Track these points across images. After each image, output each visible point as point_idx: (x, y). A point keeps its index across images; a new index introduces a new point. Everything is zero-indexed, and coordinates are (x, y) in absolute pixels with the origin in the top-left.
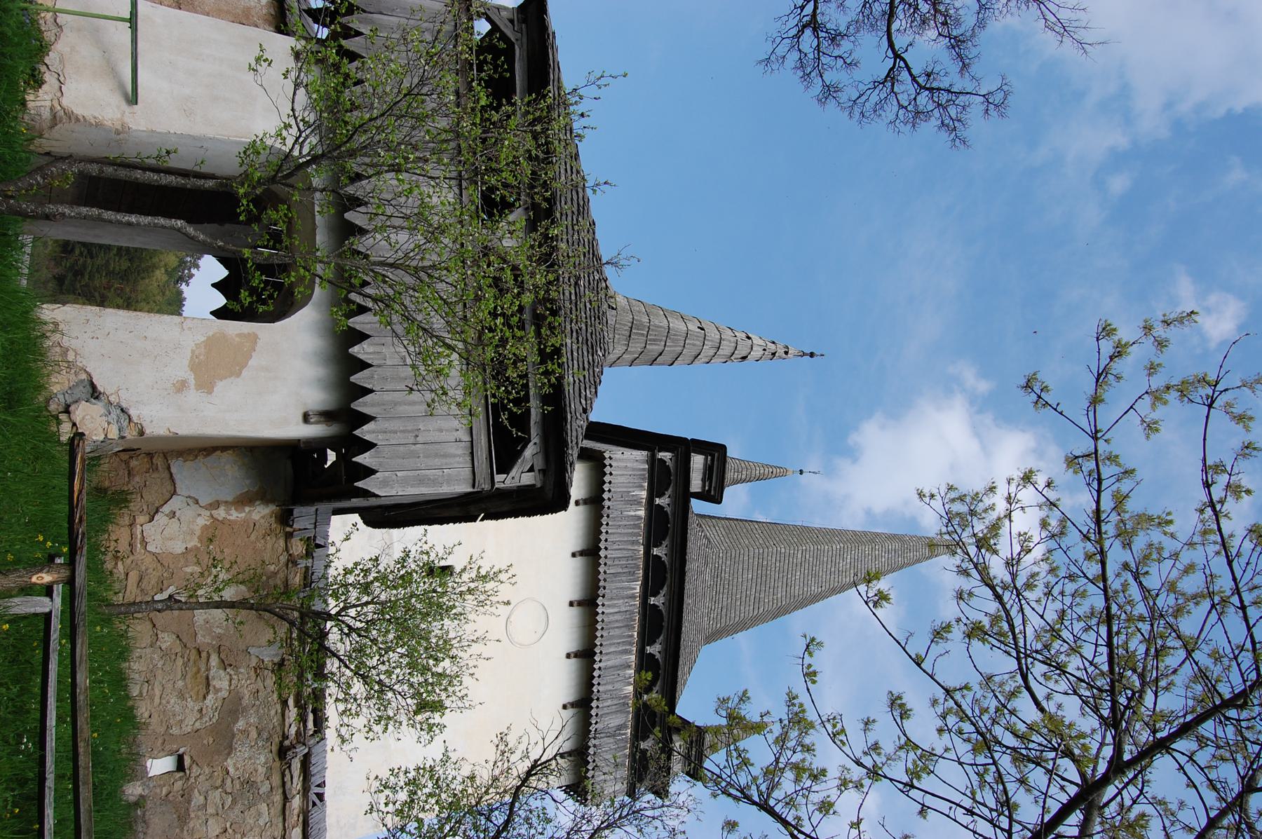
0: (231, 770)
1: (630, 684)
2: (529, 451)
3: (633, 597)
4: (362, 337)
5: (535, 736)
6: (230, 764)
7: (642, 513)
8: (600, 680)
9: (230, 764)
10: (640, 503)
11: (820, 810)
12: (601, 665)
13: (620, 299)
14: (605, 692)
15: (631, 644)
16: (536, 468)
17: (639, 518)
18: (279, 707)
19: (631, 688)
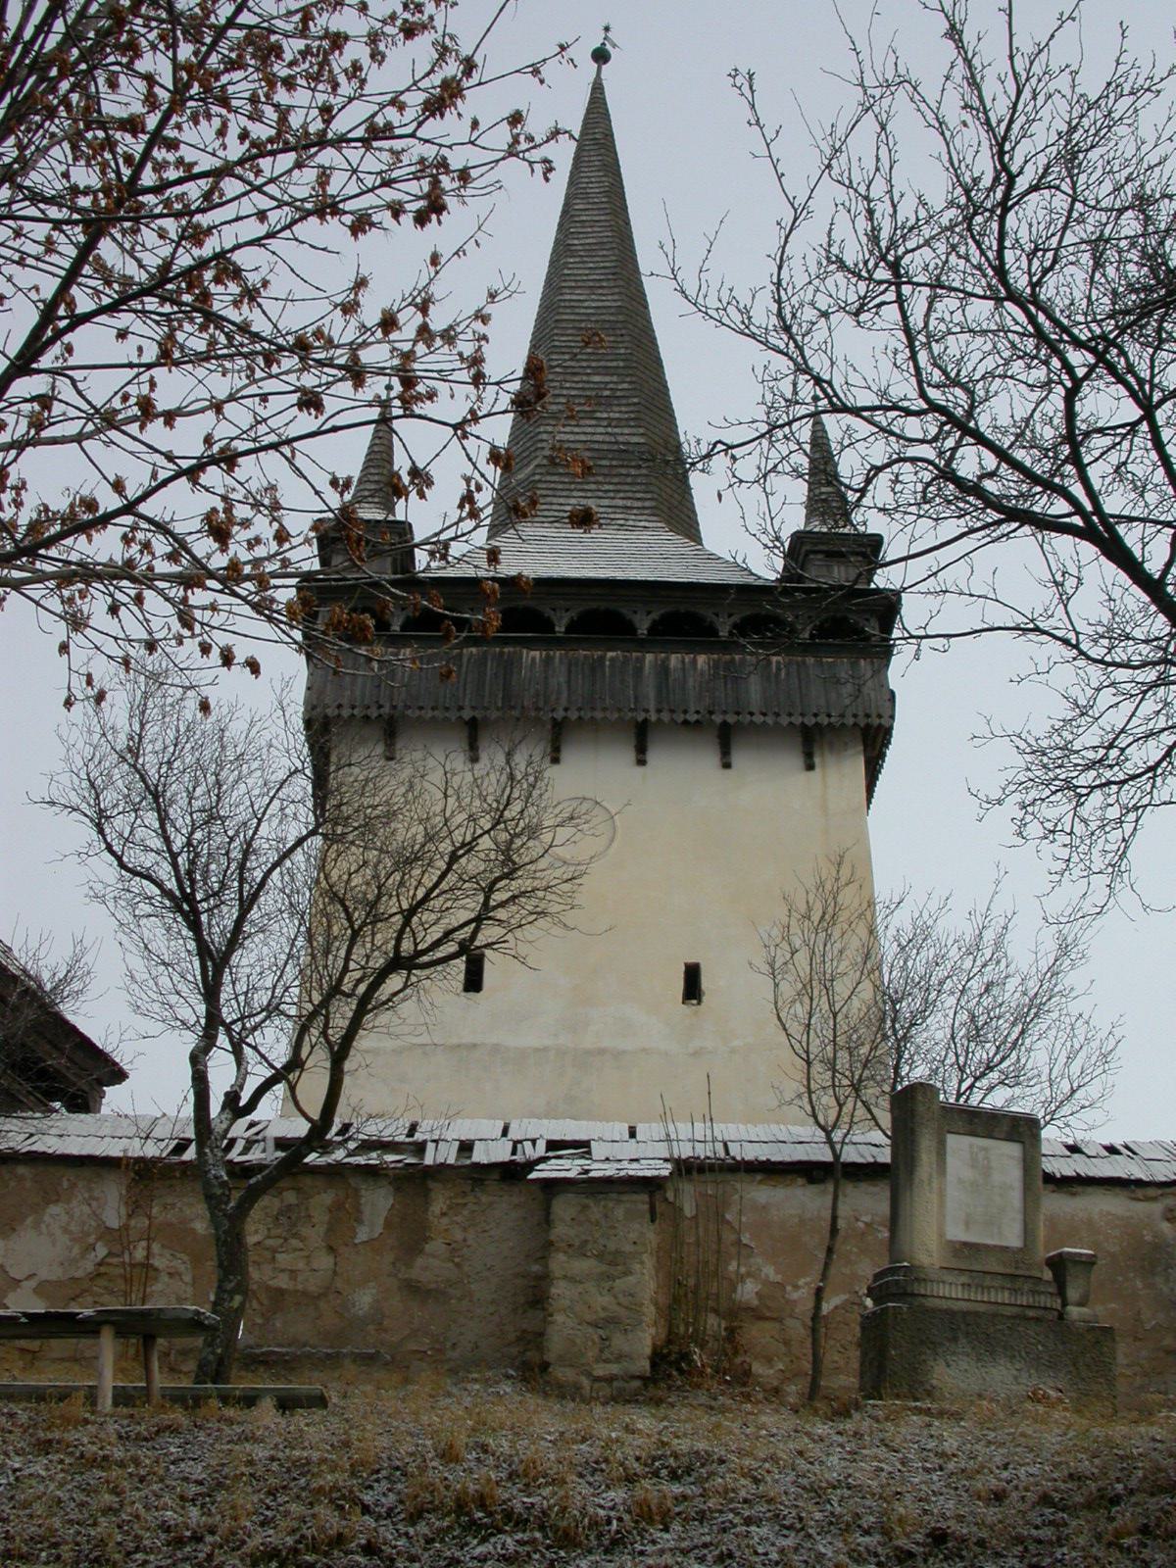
1: (694, 662)
3: (548, 662)
8: (861, 714)
19: (701, 659)
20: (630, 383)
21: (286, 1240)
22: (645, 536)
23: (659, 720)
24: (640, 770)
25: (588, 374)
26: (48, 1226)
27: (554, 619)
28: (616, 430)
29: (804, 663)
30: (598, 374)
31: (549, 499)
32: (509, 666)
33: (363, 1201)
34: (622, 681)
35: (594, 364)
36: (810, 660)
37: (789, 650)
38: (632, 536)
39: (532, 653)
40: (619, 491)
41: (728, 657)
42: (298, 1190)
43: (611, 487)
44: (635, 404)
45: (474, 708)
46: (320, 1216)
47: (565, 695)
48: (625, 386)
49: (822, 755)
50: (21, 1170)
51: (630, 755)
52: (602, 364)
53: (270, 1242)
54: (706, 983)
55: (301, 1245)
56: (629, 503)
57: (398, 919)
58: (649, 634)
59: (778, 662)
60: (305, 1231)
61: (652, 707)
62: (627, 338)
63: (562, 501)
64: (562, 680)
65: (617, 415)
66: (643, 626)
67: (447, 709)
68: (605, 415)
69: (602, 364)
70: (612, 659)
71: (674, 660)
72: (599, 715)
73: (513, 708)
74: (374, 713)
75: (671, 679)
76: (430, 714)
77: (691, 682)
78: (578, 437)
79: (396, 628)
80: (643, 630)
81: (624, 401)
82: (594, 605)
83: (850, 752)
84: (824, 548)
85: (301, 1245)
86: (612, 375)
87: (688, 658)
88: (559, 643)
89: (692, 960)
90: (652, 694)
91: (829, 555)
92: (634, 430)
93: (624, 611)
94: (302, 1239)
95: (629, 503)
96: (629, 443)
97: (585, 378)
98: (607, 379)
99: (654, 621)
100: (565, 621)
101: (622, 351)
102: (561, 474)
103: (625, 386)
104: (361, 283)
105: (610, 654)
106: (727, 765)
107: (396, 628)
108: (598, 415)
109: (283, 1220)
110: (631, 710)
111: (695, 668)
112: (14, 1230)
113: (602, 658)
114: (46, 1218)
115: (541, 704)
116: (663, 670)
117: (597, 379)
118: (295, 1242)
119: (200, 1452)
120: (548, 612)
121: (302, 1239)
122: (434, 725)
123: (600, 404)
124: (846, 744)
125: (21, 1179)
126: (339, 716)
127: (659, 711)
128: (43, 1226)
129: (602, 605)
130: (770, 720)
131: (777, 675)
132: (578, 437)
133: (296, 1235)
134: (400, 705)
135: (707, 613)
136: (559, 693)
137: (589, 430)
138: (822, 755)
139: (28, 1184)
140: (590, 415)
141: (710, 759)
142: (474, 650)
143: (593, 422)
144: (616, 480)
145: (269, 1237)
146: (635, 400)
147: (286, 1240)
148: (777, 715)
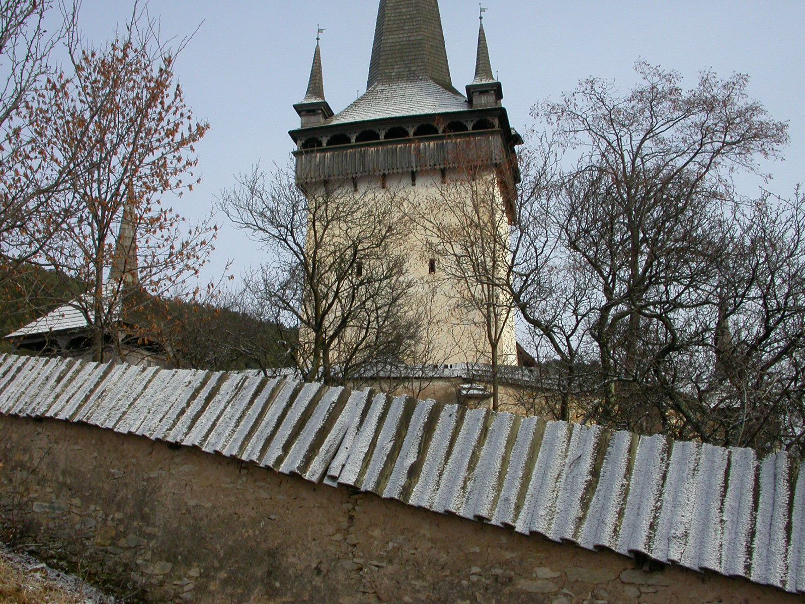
1: (429, 144)
19: (432, 143)
23: (389, 173)
32: (363, 156)
57: (735, 222)
66: (411, 132)
70: (400, 148)
79: (324, 145)
82: (393, 126)
87: (427, 144)
88: (381, 144)
99: (310, 139)
100: (354, 138)
104: (84, 53)
107: (324, 145)
116: (418, 150)
119: (559, 452)
120: (377, 131)
122: (399, 176)
135: (462, 121)
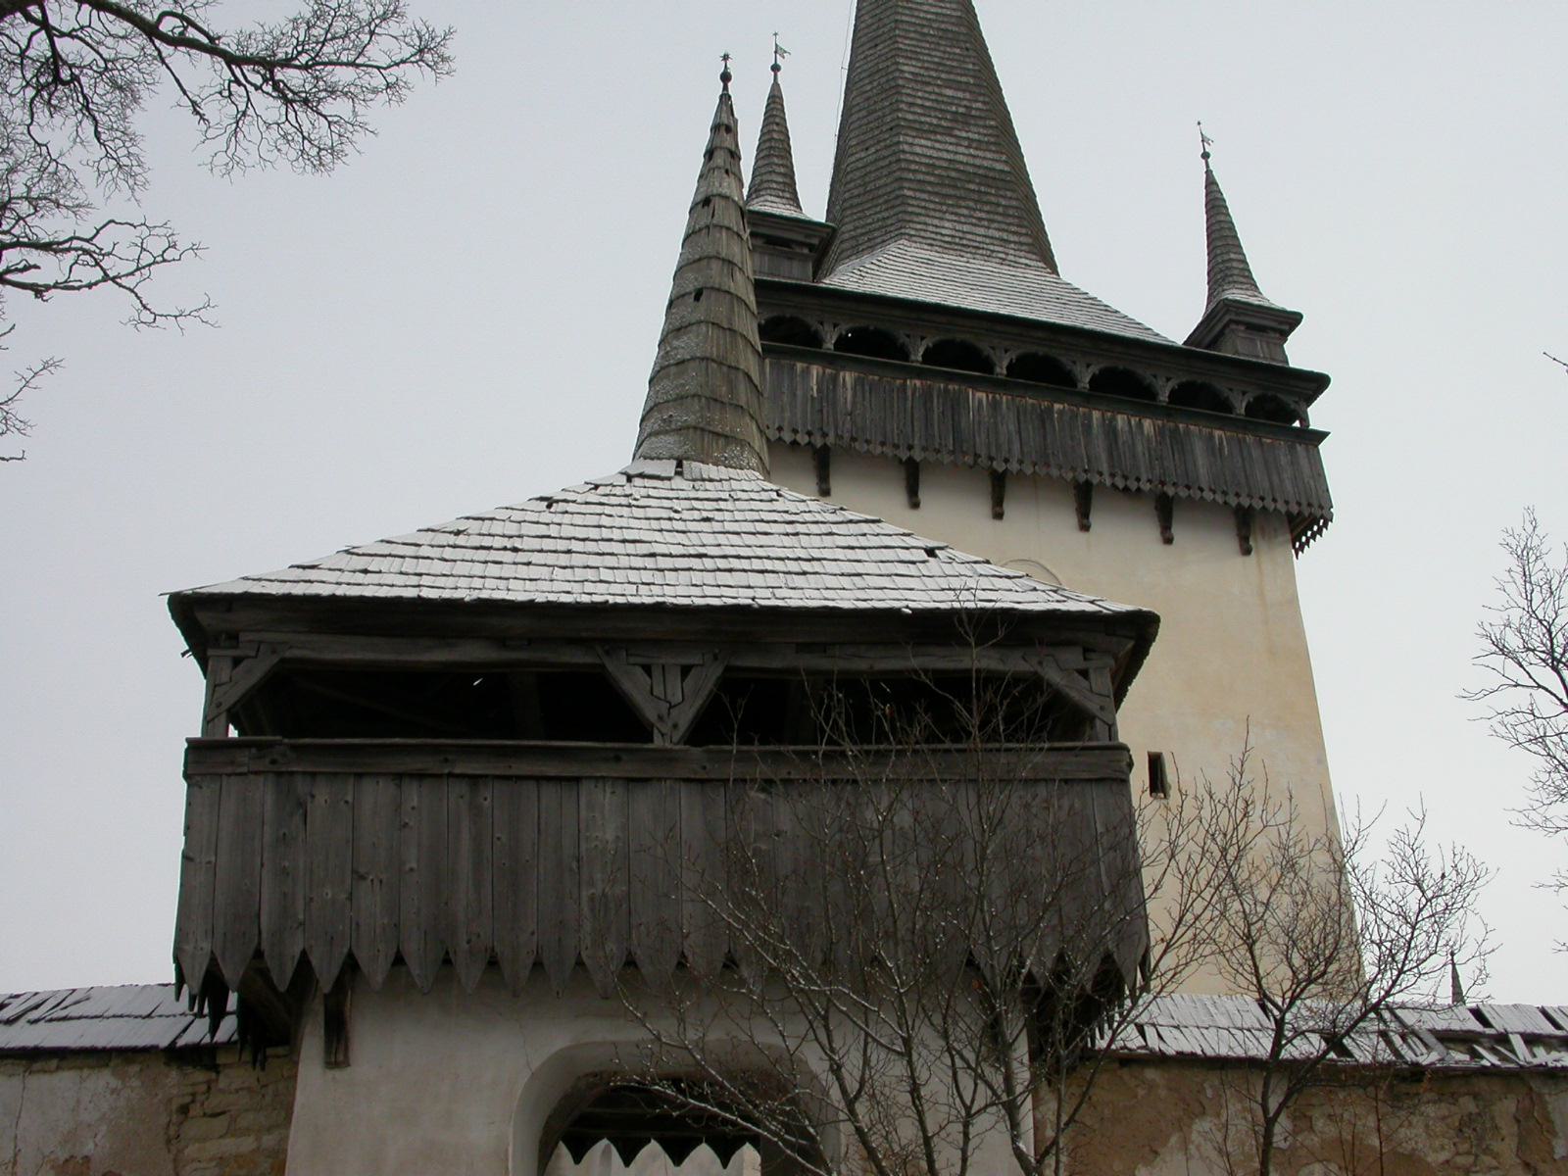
0: (1444, 1156)
1: (1140, 425)
2: (1053, 675)
3: (995, 405)
4: (700, 401)
5: (1520, 698)
6: (1435, 1158)
7: (848, 377)
8: (1304, 503)
9: (1435, 1158)
10: (834, 379)
11: (236, 638)
12: (1304, 503)
13: (282, 164)
14: (1152, 468)
15: (1075, 416)
16: (1082, 665)
17: (857, 382)
18: (1243, 950)
19: (1147, 423)
20: (984, 103)
21: (1477, 1156)
22: (1030, 274)
24: (1083, 536)
25: (938, 86)
26: (1198, 1147)
27: (995, 359)
28: (980, 153)
29: (1245, 439)
30: (950, 88)
31: (922, 219)
32: (956, 405)
33: (1550, 1107)
34: (1072, 438)
35: (943, 76)
36: (1250, 439)
37: (1226, 423)
38: (1019, 272)
39: (979, 395)
40: (993, 221)
41: (1172, 424)
42: (1476, 1096)
43: (984, 215)
44: (991, 127)
45: (924, 449)
46: (1508, 1128)
47: (1016, 446)
48: (979, 105)
49: (1256, 541)
50: (1151, 1074)
51: (1073, 520)
52: (952, 77)
53: (1460, 1160)
54: (1170, 776)
55: (1494, 1163)
56: (1005, 236)
58: (1170, 402)
59: (1220, 438)
60: (1496, 1146)
61: (1105, 468)
62: (971, 53)
63: (936, 222)
64: (1012, 427)
65: (976, 137)
67: (896, 446)
68: (964, 134)
69: (952, 77)
70: (1061, 412)
71: (1121, 420)
72: (1055, 472)
73: (964, 453)
74: (803, 439)
75: (1120, 442)
76: (879, 449)
77: (1140, 448)
78: (940, 154)
80: (1084, 381)
81: (981, 123)
82: (1033, 349)
83: (1281, 539)
84: (1247, 319)
85: (1494, 1163)
86: (964, 91)
87: (1134, 421)
89: (1155, 750)
90: (1104, 457)
91: (1250, 327)
92: (996, 156)
93: (1063, 359)
94: (1496, 1156)
95: (1005, 236)
96: (994, 170)
97: (937, 90)
98: (960, 94)
101: (971, 66)
102: (929, 192)
103: (979, 105)
105: (1057, 406)
106: (1168, 541)
108: (958, 133)
109: (1468, 1132)
110: (1085, 471)
111: (1142, 433)
112: (1156, 1153)
113: (1050, 410)
114: (1194, 1136)
115: (993, 454)
116: (1111, 432)
117: (949, 92)
118: (1487, 1160)
121: (1496, 1156)
123: (956, 121)
124: (1275, 530)
125: (1151, 1086)
126: (780, 439)
127: (1113, 475)
128: (1192, 1147)
129: (1042, 351)
130: (1220, 499)
131: (1221, 449)
132: (940, 154)
133: (1487, 1151)
134: (847, 436)
136: (1010, 442)
137: (951, 148)
138: (1256, 541)
139: (1163, 1093)
140: (949, 132)
141: (1151, 532)
142: (918, 383)
143: (953, 140)
144: (987, 208)
145: (1458, 1154)
146: (992, 123)
147: (1477, 1156)
148: (1225, 493)
